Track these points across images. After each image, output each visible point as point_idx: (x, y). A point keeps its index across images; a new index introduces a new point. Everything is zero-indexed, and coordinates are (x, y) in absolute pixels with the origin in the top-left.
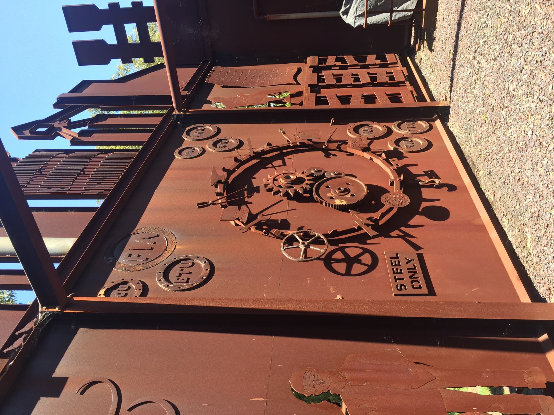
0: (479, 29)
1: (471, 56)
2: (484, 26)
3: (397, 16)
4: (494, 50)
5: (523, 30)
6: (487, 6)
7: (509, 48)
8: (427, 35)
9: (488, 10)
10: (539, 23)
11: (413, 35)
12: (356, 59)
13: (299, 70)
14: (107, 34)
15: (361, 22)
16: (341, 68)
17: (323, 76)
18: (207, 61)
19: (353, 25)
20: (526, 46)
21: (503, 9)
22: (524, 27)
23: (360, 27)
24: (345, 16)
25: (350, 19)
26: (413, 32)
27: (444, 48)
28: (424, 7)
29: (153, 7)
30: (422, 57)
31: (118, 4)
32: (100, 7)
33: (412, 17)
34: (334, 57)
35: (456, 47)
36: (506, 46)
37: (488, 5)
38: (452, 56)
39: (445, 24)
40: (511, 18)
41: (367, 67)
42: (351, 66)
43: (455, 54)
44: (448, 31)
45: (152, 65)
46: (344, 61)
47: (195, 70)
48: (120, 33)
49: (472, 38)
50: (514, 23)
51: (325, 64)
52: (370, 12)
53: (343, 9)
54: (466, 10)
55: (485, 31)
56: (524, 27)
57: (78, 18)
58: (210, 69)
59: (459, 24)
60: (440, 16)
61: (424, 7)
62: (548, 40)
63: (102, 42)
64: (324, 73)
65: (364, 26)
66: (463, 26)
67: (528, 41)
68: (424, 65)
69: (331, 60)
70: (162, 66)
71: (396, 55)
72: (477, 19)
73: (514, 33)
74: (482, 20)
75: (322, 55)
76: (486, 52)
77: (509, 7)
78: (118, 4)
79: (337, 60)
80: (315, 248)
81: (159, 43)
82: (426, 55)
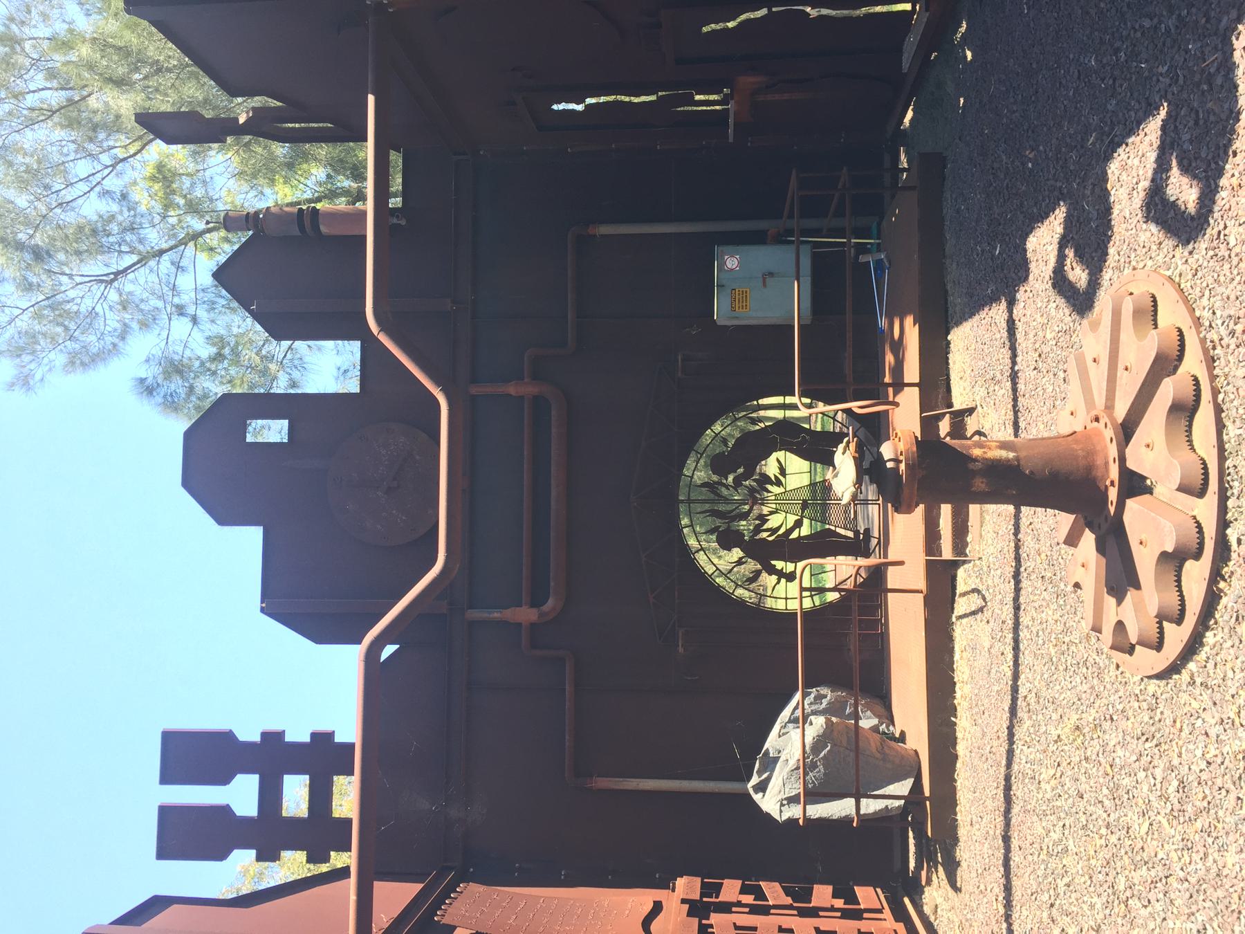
0: (1049, 855)
1: (1045, 915)
2: (1060, 848)
3: (870, 806)
4: (1092, 906)
5: (1145, 868)
6: (1058, 807)
7: (1123, 906)
8: (942, 848)
9: (1063, 815)
10: (1174, 856)
11: (912, 849)
12: (788, 892)
13: (657, 908)
14: (242, 794)
15: (795, 812)
16: (754, 910)
17: (711, 926)
18: (450, 869)
19: (777, 817)
20: (1158, 907)
21: (1094, 817)
22: (1146, 863)
23: (792, 822)
24: (760, 794)
25: (769, 803)
26: (911, 841)
27: (982, 887)
28: (927, 793)
29: (352, 746)
30: (939, 901)
31: (281, 734)
32: (243, 736)
33: (904, 811)
34: (738, 883)
35: (1008, 889)
36: (1116, 902)
37: (1058, 803)
38: (1002, 910)
39: (978, 835)
40: (1113, 839)
41: (814, 913)
42: (775, 907)
43: (1008, 905)
44: (985, 850)
45: (324, 868)
46: (760, 895)
47: (417, 888)
48: (270, 795)
49: (1040, 873)
50: (1123, 851)
51: (717, 897)
52: (814, 795)
53: (755, 780)
54: (1016, 810)
55: (1064, 862)
56: (1146, 863)
57: (194, 755)
58: (452, 887)
59: (1006, 839)
60: (964, 813)
61: (927, 793)
62: (1202, 897)
63: (225, 810)
64: (715, 918)
65: (801, 822)
66: (1015, 843)
67: (1161, 896)
68: (946, 921)
69: (731, 890)
70: (343, 873)
71: (879, 890)
72: (1040, 831)
73: (1127, 872)
74: (1055, 836)
75: (712, 872)
76: (1075, 909)
77: (1105, 815)
78: (281, 734)
79: (744, 891)
80: (627, 99)
81: (348, 821)
82: (947, 899)
